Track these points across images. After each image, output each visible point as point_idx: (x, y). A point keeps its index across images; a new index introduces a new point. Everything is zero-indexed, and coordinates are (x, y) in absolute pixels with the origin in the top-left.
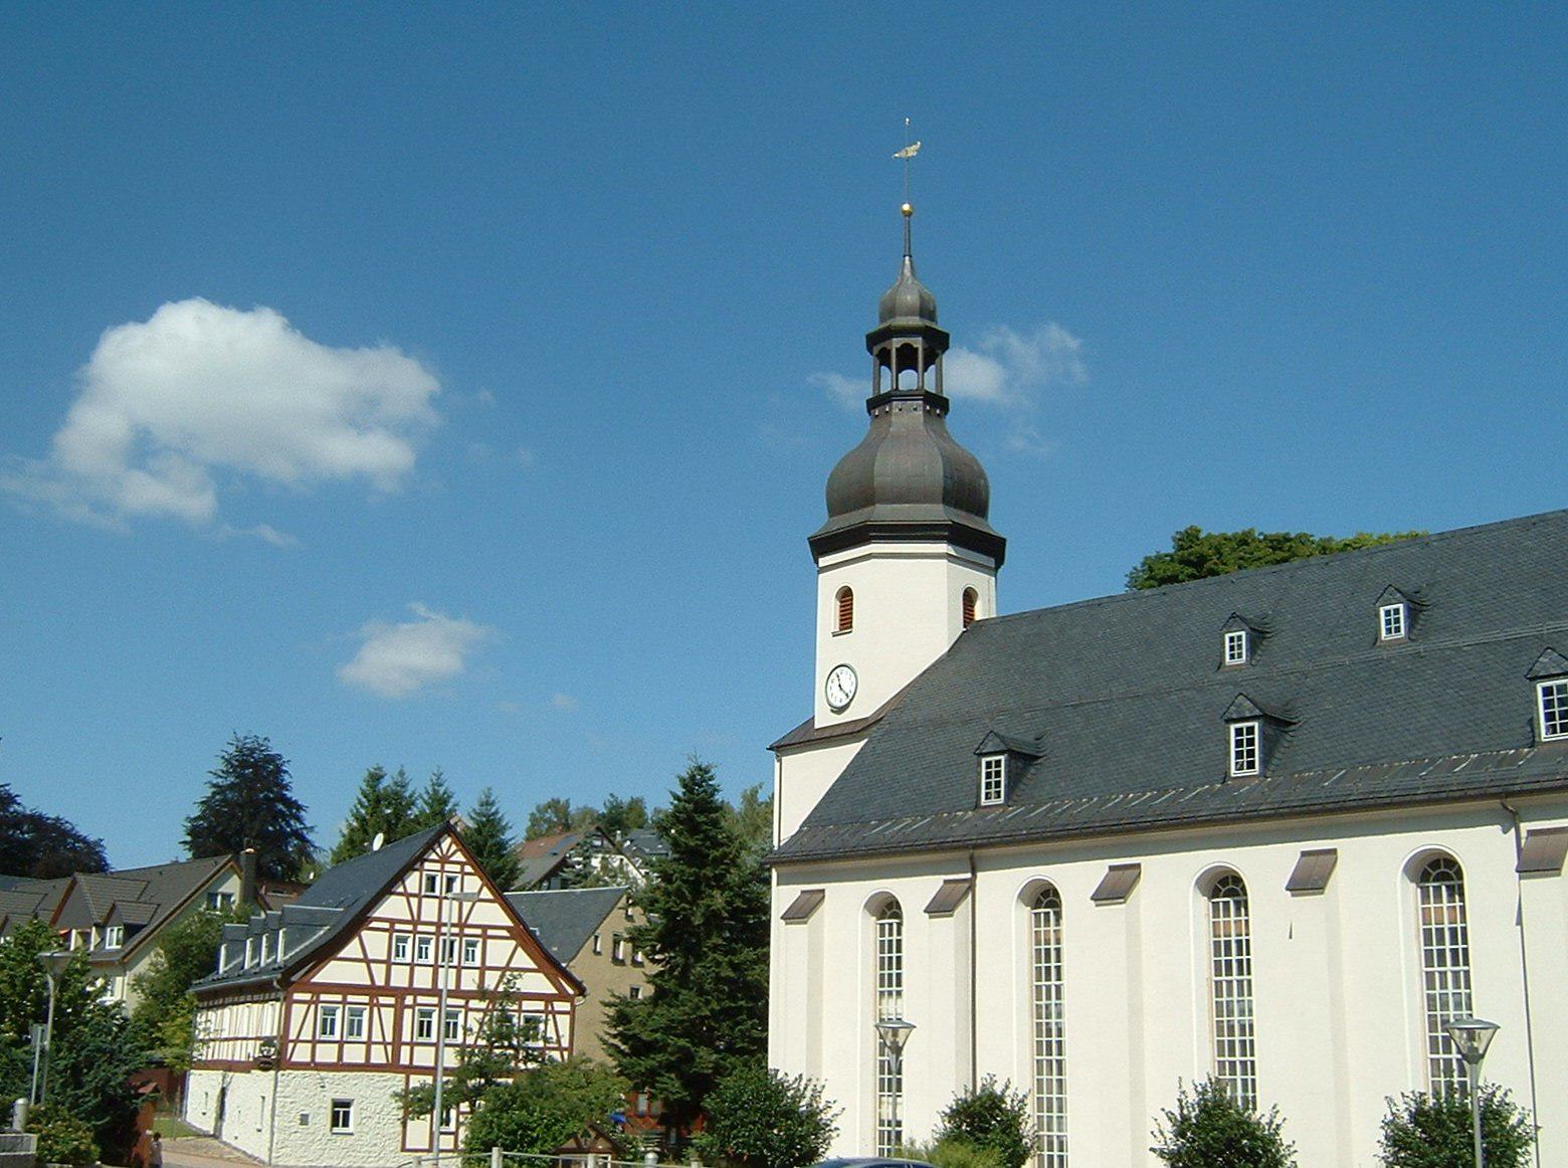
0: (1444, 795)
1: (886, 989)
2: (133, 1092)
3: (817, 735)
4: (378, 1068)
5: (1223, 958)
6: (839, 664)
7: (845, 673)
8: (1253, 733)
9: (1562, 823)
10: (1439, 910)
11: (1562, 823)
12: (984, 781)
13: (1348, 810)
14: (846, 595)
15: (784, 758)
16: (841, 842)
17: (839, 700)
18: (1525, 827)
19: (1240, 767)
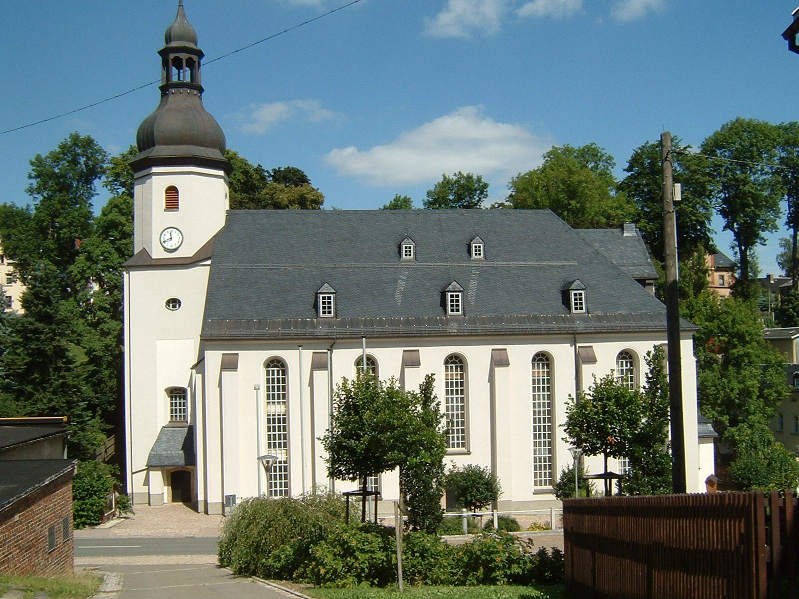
0: (552, 332)
1: (271, 401)
2: (659, 386)
3: (153, 263)
4: (178, 422)
5: (450, 388)
6: (163, 230)
7: (175, 233)
8: (325, 297)
9: (798, 335)
10: (539, 372)
11: (798, 335)
12: (460, 303)
13: (516, 335)
14: (172, 192)
15: (131, 272)
16: (55, 323)
17: (170, 245)
18: (578, 345)
19: (452, 310)
